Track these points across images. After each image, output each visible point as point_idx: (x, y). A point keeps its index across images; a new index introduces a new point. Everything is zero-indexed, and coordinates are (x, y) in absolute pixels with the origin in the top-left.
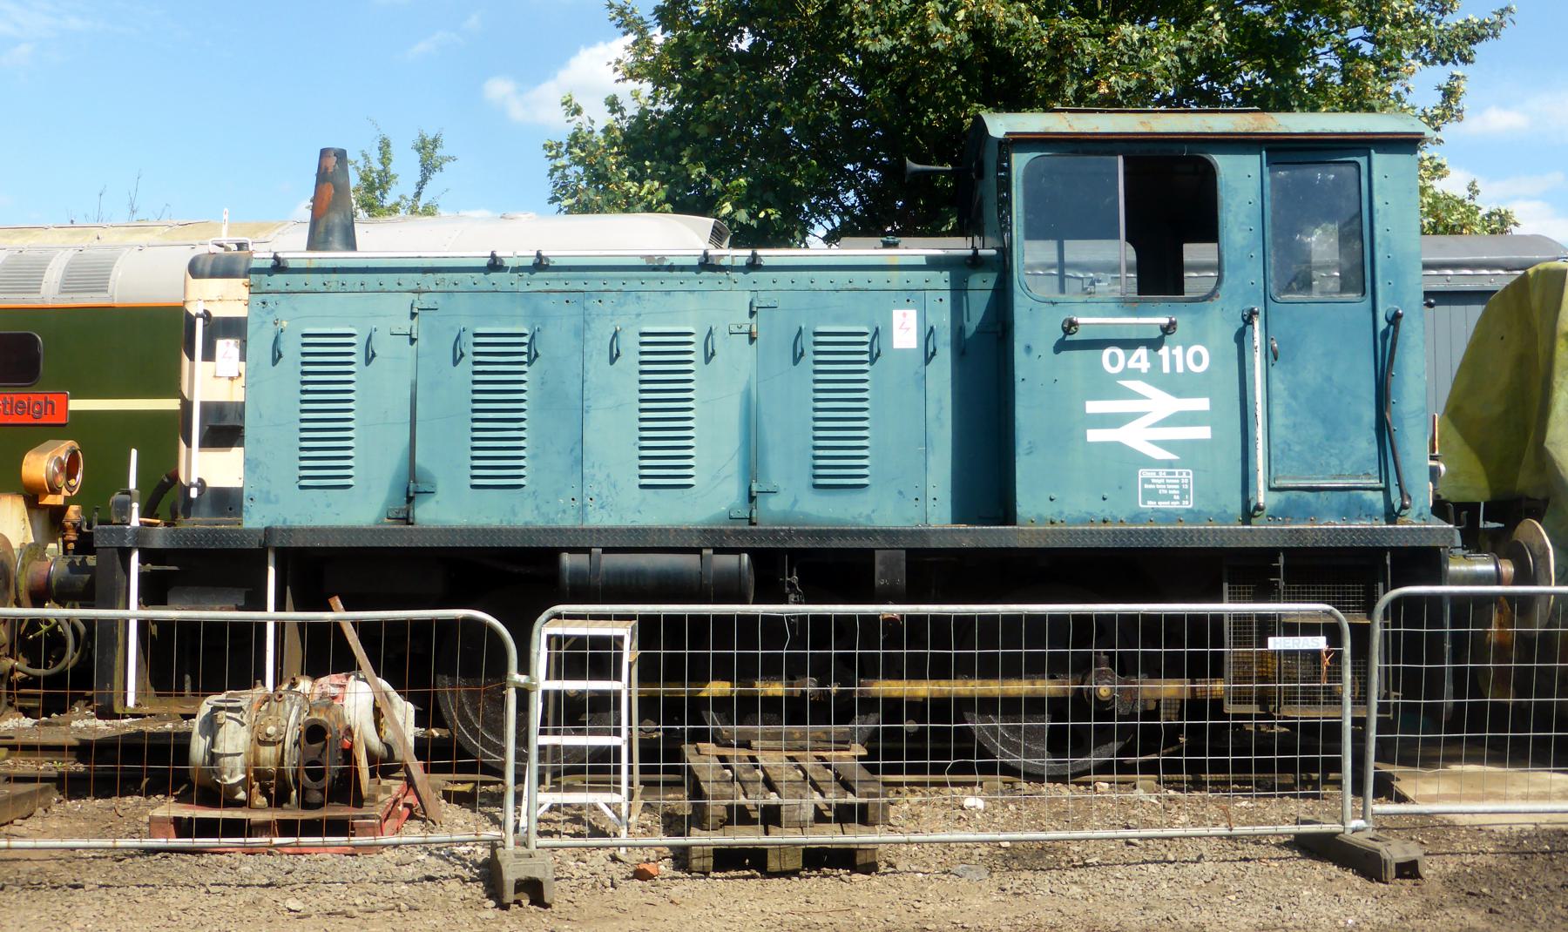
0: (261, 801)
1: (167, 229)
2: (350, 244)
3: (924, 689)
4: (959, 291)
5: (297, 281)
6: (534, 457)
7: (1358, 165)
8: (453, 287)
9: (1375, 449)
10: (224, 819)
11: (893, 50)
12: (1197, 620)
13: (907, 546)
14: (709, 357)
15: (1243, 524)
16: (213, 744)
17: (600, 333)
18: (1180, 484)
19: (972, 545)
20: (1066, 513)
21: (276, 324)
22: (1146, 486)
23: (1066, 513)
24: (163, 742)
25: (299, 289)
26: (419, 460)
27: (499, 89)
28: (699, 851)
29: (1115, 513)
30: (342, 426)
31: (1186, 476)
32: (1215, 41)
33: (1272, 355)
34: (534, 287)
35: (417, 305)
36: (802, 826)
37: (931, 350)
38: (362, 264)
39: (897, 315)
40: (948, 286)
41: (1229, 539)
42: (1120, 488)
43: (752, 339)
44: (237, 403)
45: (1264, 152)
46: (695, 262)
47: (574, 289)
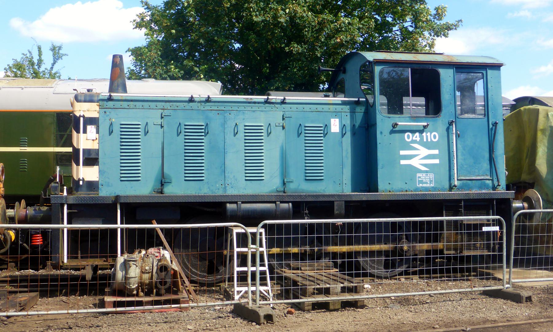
0: (141, 294)
1: (8, 81)
2: (125, 91)
3: (345, 249)
4: (353, 112)
5: (118, 104)
6: (207, 170)
7: (483, 74)
8: (176, 108)
9: (489, 167)
12: (436, 222)
13: (345, 200)
14: (269, 134)
15: (449, 191)
17: (231, 125)
18: (430, 178)
19: (366, 199)
21: (110, 120)
22: (419, 179)
26: (165, 170)
27: (16, 23)
29: (410, 188)
30: (136, 158)
31: (432, 176)
32: (371, 26)
33: (458, 136)
34: (206, 108)
35: (163, 114)
36: (337, 294)
37: (146, 131)
39: (332, 120)
40: (349, 111)
42: (411, 180)
43: (283, 128)
44: (95, 149)
45: (455, 69)
46: (187, 99)
47: (220, 109)
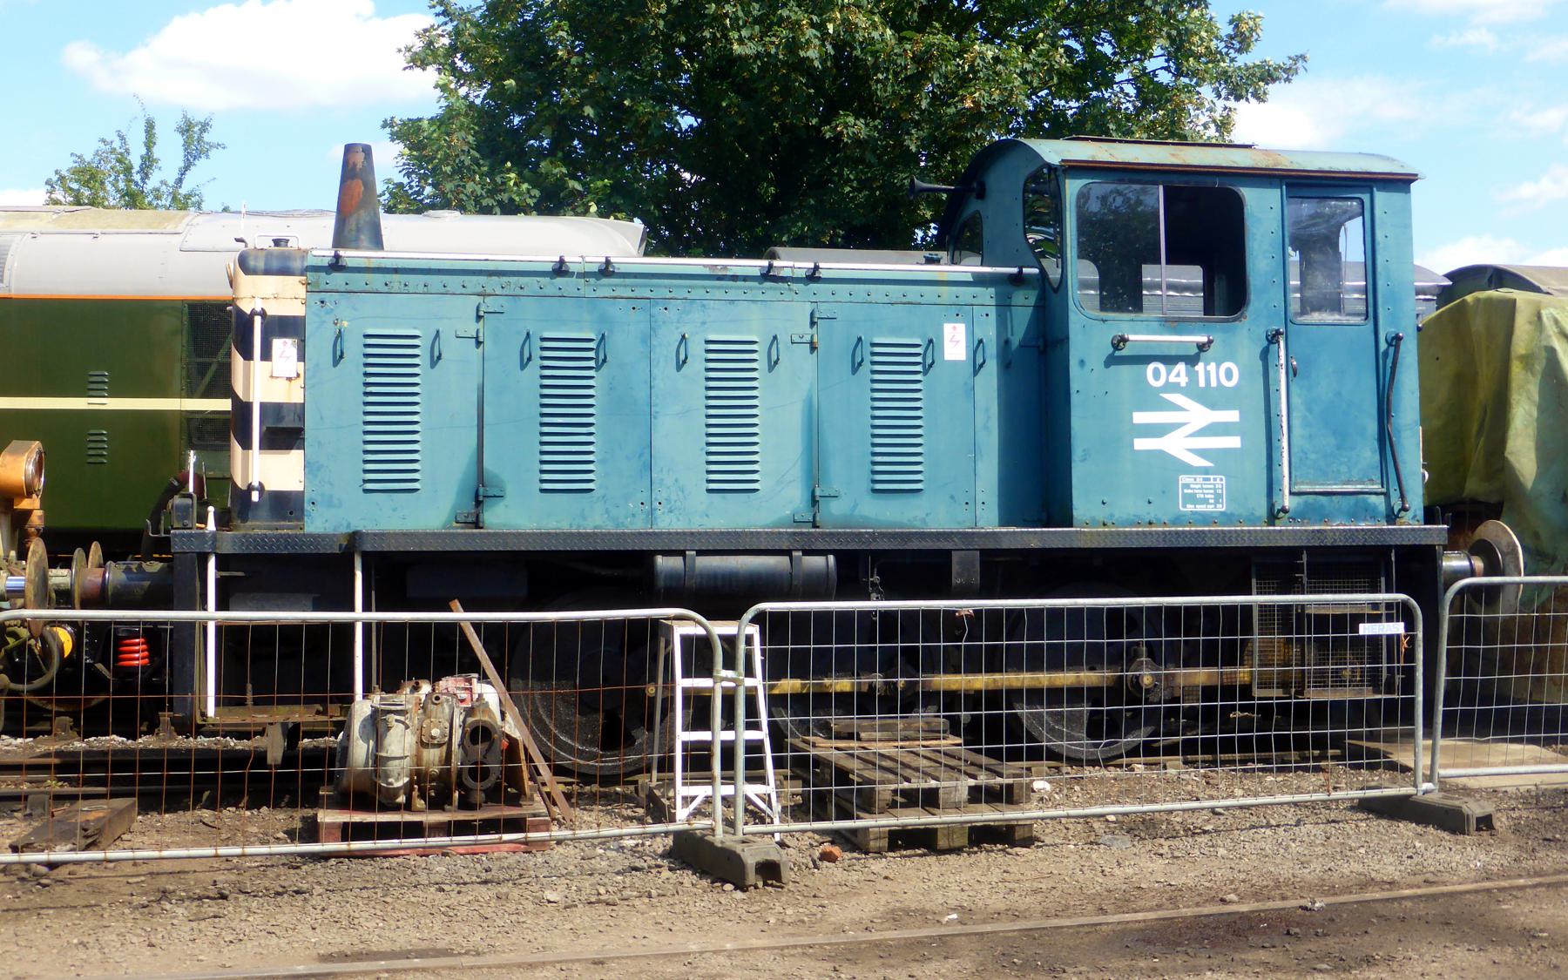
2: (378, 243)
3: (981, 681)
4: (1003, 305)
5: (358, 280)
6: (603, 461)
9: (1377, 457)
10: (455, 821)
11: (758, 56)
12: (1230, 610)
13: (982, 547)
14: (773, 365)
16: (379, 745)
18: (1215, 489)
20: (1117, 516)
21: (336, 324)
22: (1186, 491)
23: (1117, 516)
24: (102, 758)
25: (360, 290)
26: (487, 464)
28: (876, 833)
30: (408, 428)
31: (1220, 482)
33: (1292, 372)
34: (600, 293)
35: (483, 308)
36: (957, 807)
38: (389, 264)
39: (948, 328)
41: (1262, 539)
42: (1164, 492)
43: (813, 348)
